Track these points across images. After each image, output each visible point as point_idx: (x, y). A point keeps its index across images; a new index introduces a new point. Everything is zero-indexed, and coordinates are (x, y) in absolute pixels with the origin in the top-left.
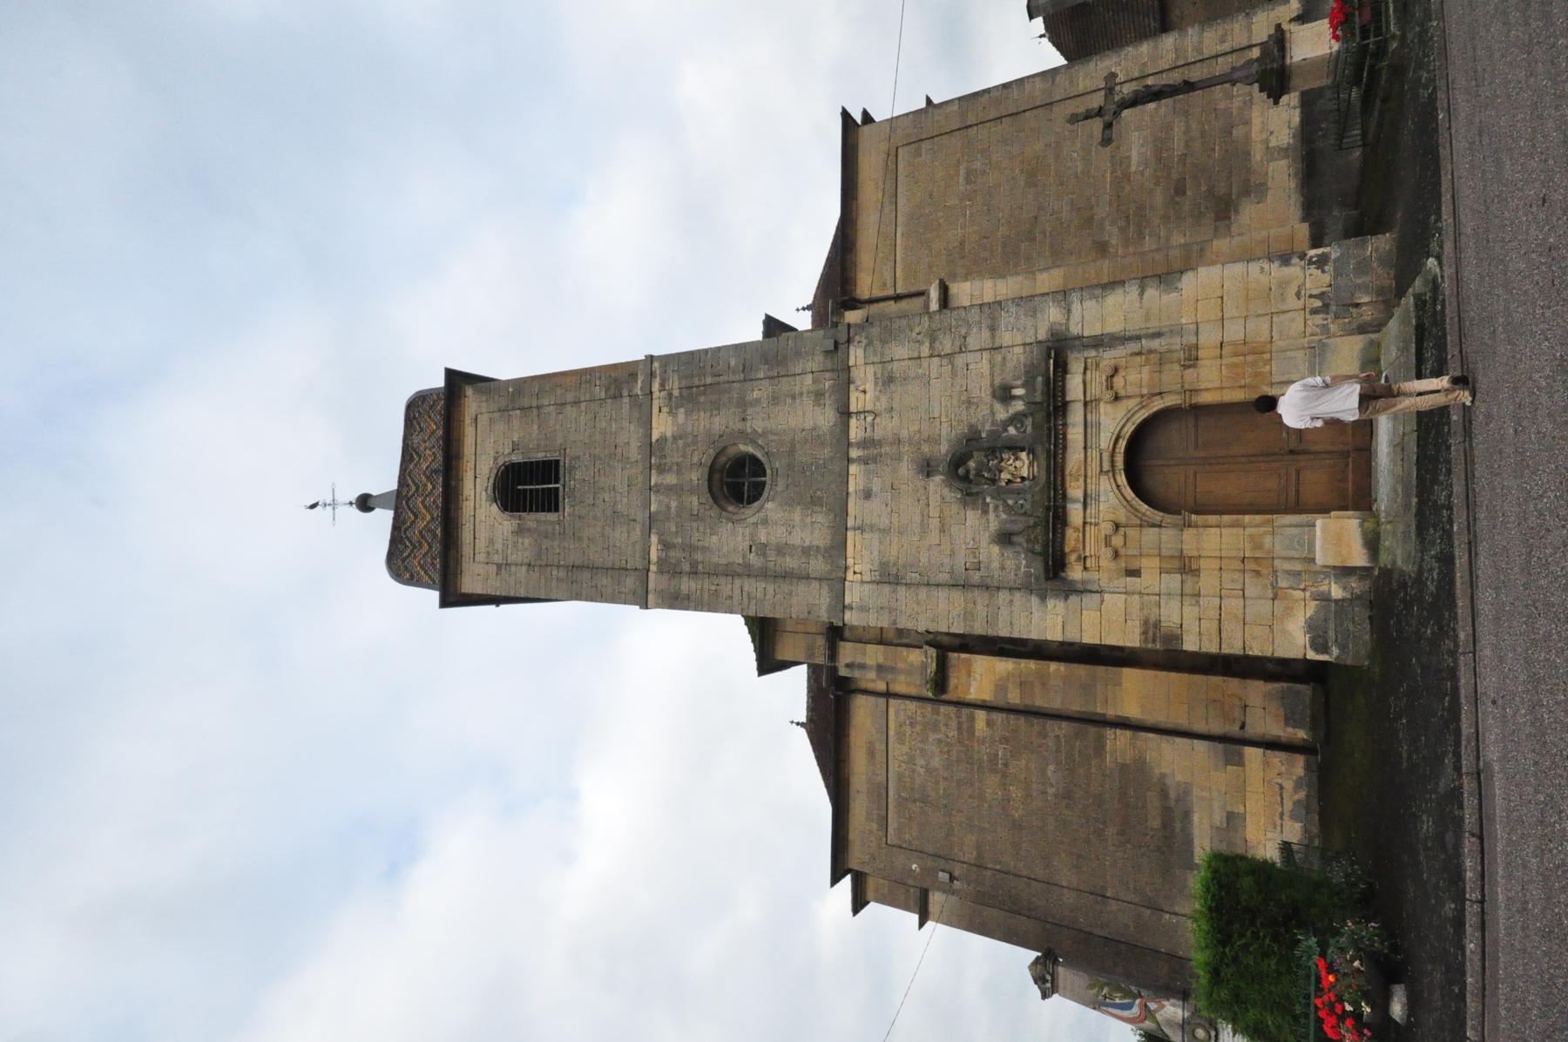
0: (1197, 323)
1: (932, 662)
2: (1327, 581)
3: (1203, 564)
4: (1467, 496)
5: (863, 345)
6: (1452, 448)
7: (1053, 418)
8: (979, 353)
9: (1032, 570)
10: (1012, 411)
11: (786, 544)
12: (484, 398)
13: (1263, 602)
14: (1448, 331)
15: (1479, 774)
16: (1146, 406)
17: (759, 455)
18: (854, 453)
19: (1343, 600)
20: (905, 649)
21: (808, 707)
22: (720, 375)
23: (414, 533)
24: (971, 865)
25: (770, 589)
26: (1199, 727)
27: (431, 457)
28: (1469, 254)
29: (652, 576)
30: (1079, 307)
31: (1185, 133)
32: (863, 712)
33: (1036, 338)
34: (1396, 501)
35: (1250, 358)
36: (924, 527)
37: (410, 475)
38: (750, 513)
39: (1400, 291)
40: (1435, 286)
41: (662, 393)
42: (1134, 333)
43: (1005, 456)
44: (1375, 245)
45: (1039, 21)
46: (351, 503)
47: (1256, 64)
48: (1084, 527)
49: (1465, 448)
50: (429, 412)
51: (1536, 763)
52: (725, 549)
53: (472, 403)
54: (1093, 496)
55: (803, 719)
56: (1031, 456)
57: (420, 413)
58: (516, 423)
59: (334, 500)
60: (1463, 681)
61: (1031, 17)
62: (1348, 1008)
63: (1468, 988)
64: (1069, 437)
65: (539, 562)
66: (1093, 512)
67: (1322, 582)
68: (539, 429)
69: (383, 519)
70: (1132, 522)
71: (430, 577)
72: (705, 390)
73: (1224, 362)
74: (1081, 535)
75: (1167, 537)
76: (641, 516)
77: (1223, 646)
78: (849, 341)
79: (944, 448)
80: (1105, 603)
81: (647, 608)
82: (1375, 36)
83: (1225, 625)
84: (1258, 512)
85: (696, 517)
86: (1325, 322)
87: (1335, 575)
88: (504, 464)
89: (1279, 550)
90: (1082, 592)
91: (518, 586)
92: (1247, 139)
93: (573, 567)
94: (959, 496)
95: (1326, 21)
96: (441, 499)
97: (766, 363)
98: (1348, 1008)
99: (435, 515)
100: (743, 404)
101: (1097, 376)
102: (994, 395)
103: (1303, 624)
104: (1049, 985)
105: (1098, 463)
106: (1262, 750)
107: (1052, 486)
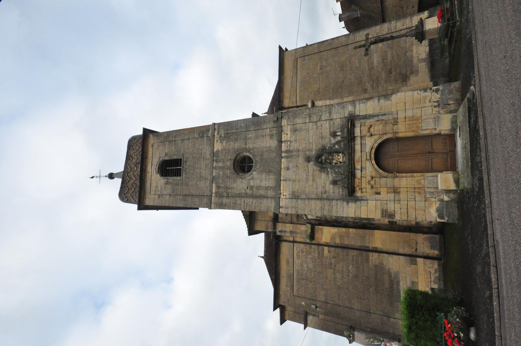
0: (397, 111)
1: (309, 229)
2: (443, 195)
3: (401, 190)
4: (486, 157)
5: (287, 119)
6: (481, 143)
7: (350, 142)
8: (325, 121)
9: (344, 193)
10: (336, 140)
11: (260, 186)
12: (156, 138)
13: (421, 202)
14: (478, 107)
15: (494, 246)
16: (381, 137)
17: (251, 156)
18: (283, 155)
19: (448, 201)
20: (300, 225)
21: (265, 251)
22: (238, 129)
23: (129, 185)
24: (323, 302)
25: (254, 202)
26: (401, 251)
27: (137, 158)
28: (484, 83)
29: (213, 198)
30: (358, 105)
31: (392, 54)
32: (285, 248)
33: (344, 116)
34: (464, 166)
35: (415, 122)
36: (307, 180)
37: (128, 165)
38: (248, 176)
39: (463, 99)
40: (474, 94)
41: (218, 135)
42: (377, 114)
43: (334, 155)
44: (454, 85)
45: (343, 23)
46: (106, 176)
47: (414, 31)
48: (361, 178)
49: (485, 143)
50: (136, 143)
51: (512, 232)
52: (239, 188)
53: (152, 140)
54: (364, 168)
55: (263, 255)
56: (343, 155)
57: (133, 143)
58: (167, 146)
59: (100, 175)
60: (488, 217)
61: (340, 21)
62: (456, 335)
63: (495, 318)
64: (356, 148)
65: (173, 194)
66: (364, 173)
67: (441, 195)
68: (175, 148)
69: (118, 181)
70: (377, 176)
71: (134, 200)
72: (233, 134)
73: (407, 123)
74: (360, 181)
75: (388, 181)
76: (209, 177)
77: (409, 218)
78: (282, 118)
79: (314, 153)
80: (368, 204)
81: (211, 209)
82: (452, 21)
83: (410, 211)
84: (418, 172)
85: (228, 177)
86: (439, 110)
87: (445, 193)
88: (162, 160)
89: (426, 184)
90: (361, 200)
91: (166, 202)
92: (412, 56)
93: (185, 195)
94: (319, 169)
95: (436, 17)
96: (139, 173)
97: (254, 125)
98: (456, 335)
99: (137, 178)
100: (246, 139)
101: (365, 128)
102: (330, 135)
103: (435, 209)
104: (352, 338)
105: (366, 157)
106: (423, 259)
107: (350, 164)
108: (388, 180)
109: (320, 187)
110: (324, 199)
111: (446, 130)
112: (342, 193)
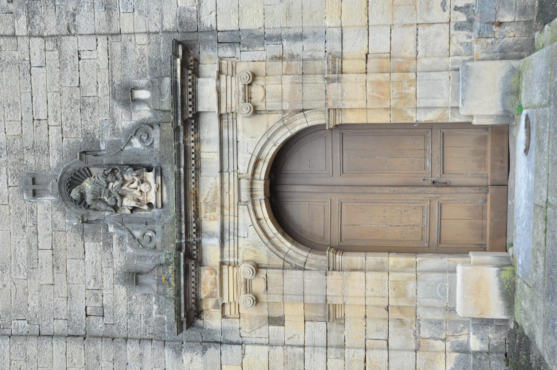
3: (349, 312)
7: (182, 134)
8: (93, 38)
16: (288, 124)
19: (481, 352)
48: (221, 269)
54: (232, 230)
56: (159, 178)
66: (232, 249)
67: (462, 331)
73: (371, 77)
74: (218, 277)
80: (246, 356)
86: (469, 40)
87: (473, 325)
108: (307, 277)
109: (82, 293)
110: (97, 337)
111: (491, 116)
112: (159, 316)
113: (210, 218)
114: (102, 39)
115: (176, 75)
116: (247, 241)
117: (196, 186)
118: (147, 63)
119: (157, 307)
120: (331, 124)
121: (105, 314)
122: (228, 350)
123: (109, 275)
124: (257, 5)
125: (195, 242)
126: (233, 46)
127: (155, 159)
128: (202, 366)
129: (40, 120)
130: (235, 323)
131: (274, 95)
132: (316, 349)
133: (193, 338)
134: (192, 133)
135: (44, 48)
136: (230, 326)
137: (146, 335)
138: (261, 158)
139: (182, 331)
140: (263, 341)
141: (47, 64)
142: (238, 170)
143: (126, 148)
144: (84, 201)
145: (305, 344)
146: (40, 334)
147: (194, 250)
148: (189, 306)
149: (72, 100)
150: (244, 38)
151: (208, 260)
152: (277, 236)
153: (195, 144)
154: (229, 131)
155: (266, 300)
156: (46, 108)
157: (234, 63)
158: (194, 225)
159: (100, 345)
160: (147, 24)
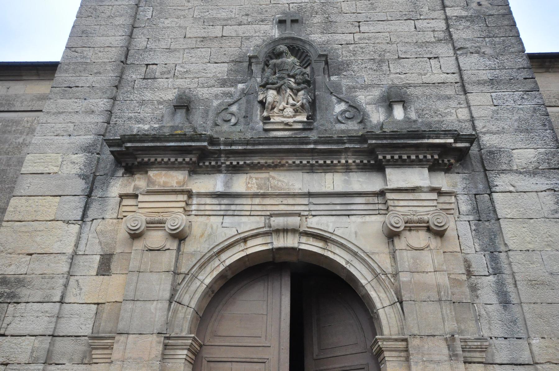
48: (182, 192)
54: (233, 207)
56: (300, 126)
107: (249, 147)
108: (160, 305)
113: (249, 183)
114: (456, 77)
115: (432, 138)
116: (218, 226)
117: (290, 166)
118: (435, 119)
119: (146, 129)
120: (385, 343)
121: (146, 80)
122: (78, 204)
123: (190, 84)
124: (538, 241)
125: (219, 163)
126: (474, 211)
127: (322, 125)
128: (65, 175)
129: (359, 27)
130: (112, 213)
131: (418, 261)
132: (54, 319)
133: (102, 165)
134: (358, 161)
135: (436, 30)
136: (109, 207)
137: (115, 118)
138: (329, 244)
139: (110, 146)
140: (82, 247)
141: (419, 33)
142: (311, 217)
143: (333, 97)
144: (274, 57)
145: (64, 304)
146: (134, 27)
147: (210, 163)
148: (139, 154)
149: (383, 52)
150: (487, 226)
151: (196, 181)
152: (221, 265)
153: (343, 165)
154: (363, 206)
155: (134, 248)
156: (372, 31)
157: (452, 212)
158: (241, 163)
159: (112, 75)
160: (483, 118)
